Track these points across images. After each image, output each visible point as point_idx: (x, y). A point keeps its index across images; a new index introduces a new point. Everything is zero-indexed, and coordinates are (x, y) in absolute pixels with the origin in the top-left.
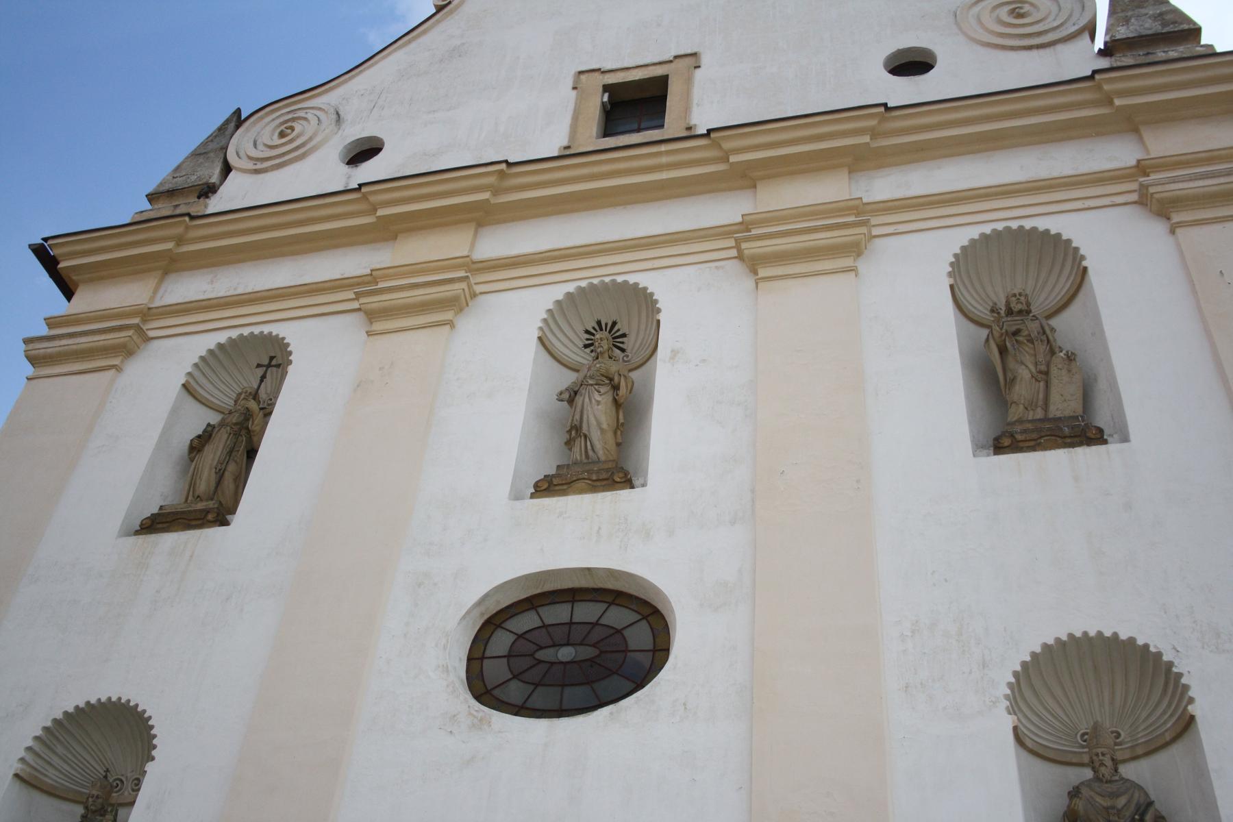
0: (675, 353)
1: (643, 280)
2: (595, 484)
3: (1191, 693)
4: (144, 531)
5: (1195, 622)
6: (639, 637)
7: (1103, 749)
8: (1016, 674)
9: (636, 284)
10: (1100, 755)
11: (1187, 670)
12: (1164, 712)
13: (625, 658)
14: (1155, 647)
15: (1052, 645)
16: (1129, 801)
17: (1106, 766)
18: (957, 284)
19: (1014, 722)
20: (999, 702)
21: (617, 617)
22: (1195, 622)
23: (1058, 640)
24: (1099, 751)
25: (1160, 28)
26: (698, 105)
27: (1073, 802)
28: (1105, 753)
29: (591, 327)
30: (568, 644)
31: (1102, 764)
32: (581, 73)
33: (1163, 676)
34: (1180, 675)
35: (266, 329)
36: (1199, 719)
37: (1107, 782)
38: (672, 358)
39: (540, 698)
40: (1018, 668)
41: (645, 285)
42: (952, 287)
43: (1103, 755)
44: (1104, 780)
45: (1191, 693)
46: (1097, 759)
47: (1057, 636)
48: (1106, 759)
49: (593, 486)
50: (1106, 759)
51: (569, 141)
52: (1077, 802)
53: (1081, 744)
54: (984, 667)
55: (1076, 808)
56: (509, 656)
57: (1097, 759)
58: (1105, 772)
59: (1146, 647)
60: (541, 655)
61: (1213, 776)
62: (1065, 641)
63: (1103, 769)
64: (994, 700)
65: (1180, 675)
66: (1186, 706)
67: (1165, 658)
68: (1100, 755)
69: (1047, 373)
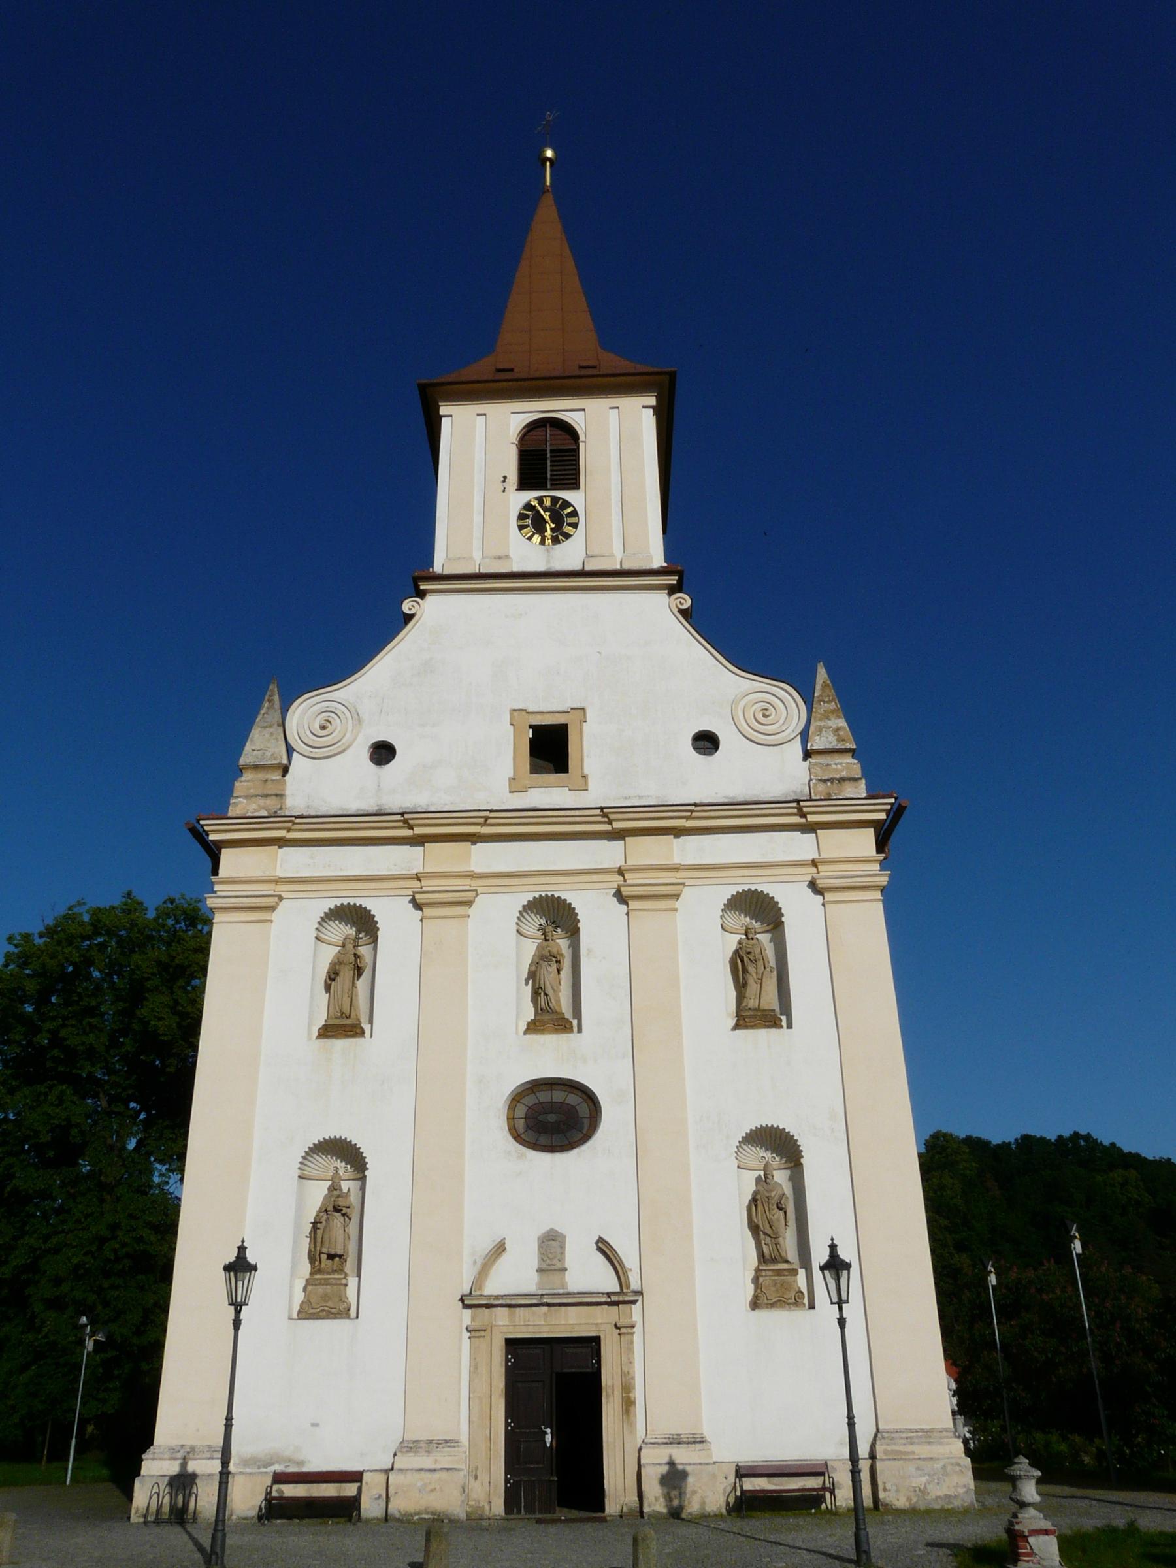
0: (589, 950)
1: (367, 904)
2: (556, 1027)
4: (322, 1037)
6: (584, 1110)
9: (559, 897)
13: (604, 1323)
16: (776, 1194)
18: (725, 923)
21: (573, 1099)
25: (836, 743)
26: (587, 756)
29: (527, 987)
30: (552, 1113)
32: (514, 710)
35: (358, 902)
38: (588, 954)
39: (543, 1140)
41: (565, 898)
49: (556, 1029)
51: (514, 775)
56: (529, 1108)
60: (539, 1118)
69: (762, 979)
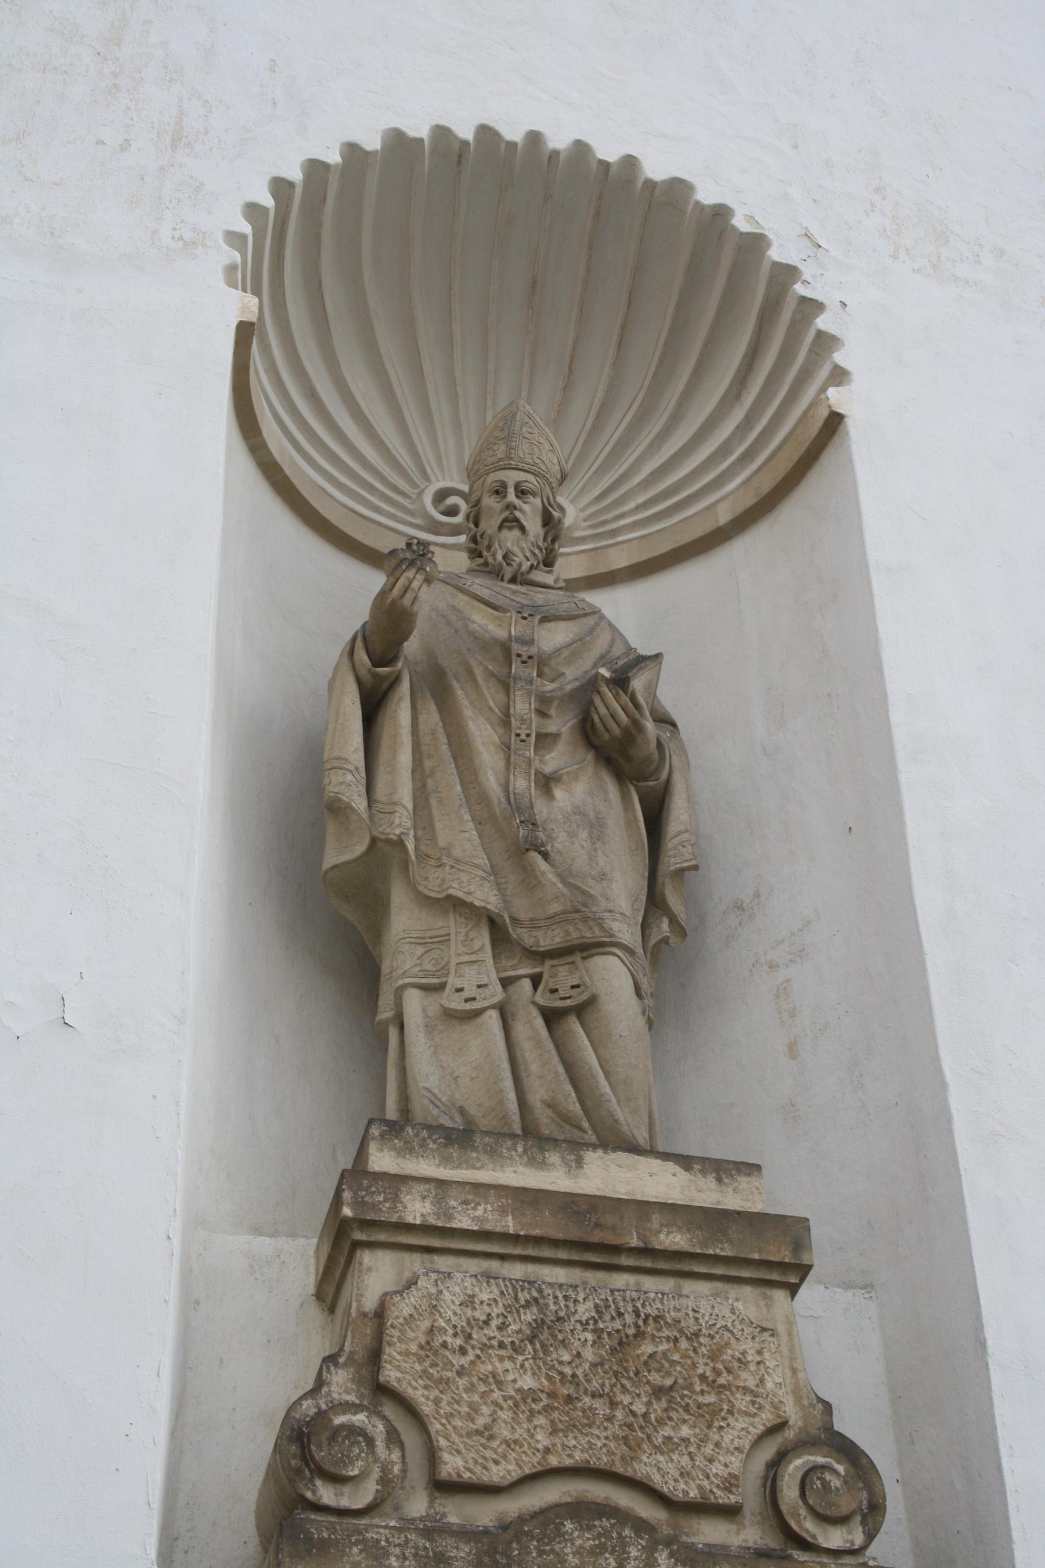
3: (839, 358)
5: (878, 190)
7: (521, 476)
8: (280, 187)
10: (511, 491)
11: (839, 297)
12: (724, 450)
14: (750, 219)
15: (420, 141)
17: (523, 529)
19: (244, 308)
20: (205, 246)
22: (878, 190)
23: (441, 133)
24: (512, 477)
27: (402, 581)
28: (526, 486)
31: (512, 522)
33: (335, 1286)
34: (811, 307)
36: (855, 427)
37: (513, 580)
40: (295, 174)
42: (245, 333)
43: (522, 492)
44: (508, 572)
45: (839, 358)
46: (498, 506)
47: (443, 123)
48: (526, 507)
50: (526, 507)
52: (416, 584)
53: (431, 518)
54: (175, 143)
55: (407, 601)
57: (498, 506)
58: (516, 550)
59: (721, 213)
61: (879, 582)
62: (465, 143)
63: (510, 538)
64: (188, 235)
65: (811, 307)
66: (823, 389)
67: (775, 254)
68: (511, 491)
